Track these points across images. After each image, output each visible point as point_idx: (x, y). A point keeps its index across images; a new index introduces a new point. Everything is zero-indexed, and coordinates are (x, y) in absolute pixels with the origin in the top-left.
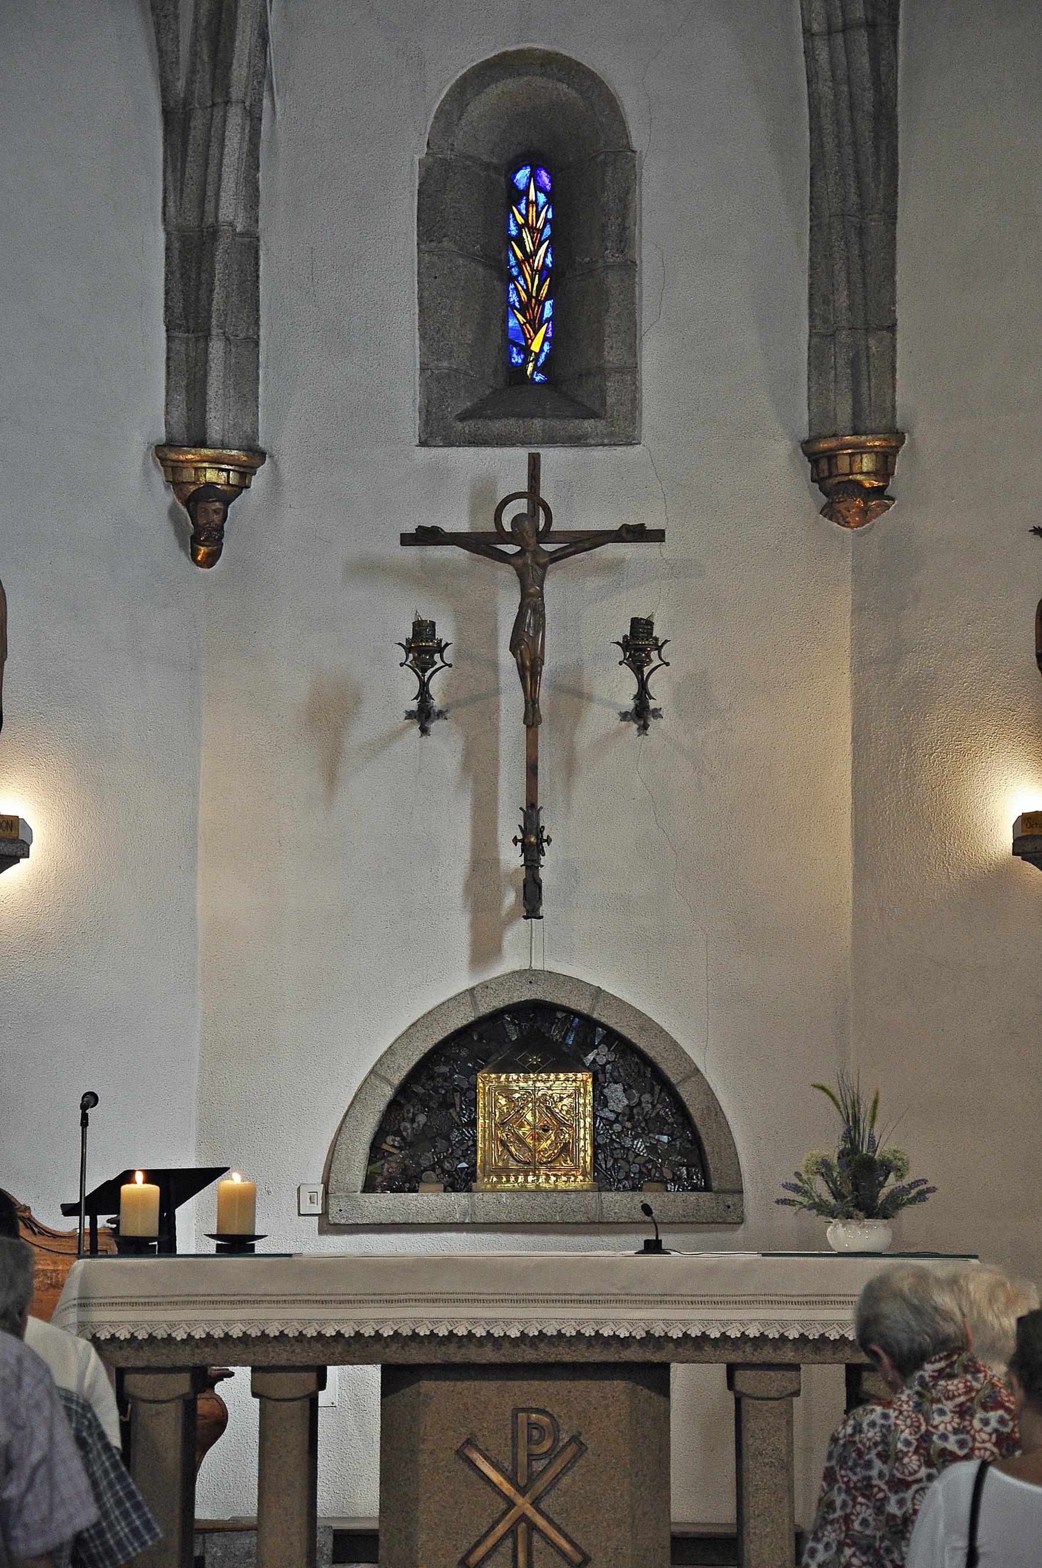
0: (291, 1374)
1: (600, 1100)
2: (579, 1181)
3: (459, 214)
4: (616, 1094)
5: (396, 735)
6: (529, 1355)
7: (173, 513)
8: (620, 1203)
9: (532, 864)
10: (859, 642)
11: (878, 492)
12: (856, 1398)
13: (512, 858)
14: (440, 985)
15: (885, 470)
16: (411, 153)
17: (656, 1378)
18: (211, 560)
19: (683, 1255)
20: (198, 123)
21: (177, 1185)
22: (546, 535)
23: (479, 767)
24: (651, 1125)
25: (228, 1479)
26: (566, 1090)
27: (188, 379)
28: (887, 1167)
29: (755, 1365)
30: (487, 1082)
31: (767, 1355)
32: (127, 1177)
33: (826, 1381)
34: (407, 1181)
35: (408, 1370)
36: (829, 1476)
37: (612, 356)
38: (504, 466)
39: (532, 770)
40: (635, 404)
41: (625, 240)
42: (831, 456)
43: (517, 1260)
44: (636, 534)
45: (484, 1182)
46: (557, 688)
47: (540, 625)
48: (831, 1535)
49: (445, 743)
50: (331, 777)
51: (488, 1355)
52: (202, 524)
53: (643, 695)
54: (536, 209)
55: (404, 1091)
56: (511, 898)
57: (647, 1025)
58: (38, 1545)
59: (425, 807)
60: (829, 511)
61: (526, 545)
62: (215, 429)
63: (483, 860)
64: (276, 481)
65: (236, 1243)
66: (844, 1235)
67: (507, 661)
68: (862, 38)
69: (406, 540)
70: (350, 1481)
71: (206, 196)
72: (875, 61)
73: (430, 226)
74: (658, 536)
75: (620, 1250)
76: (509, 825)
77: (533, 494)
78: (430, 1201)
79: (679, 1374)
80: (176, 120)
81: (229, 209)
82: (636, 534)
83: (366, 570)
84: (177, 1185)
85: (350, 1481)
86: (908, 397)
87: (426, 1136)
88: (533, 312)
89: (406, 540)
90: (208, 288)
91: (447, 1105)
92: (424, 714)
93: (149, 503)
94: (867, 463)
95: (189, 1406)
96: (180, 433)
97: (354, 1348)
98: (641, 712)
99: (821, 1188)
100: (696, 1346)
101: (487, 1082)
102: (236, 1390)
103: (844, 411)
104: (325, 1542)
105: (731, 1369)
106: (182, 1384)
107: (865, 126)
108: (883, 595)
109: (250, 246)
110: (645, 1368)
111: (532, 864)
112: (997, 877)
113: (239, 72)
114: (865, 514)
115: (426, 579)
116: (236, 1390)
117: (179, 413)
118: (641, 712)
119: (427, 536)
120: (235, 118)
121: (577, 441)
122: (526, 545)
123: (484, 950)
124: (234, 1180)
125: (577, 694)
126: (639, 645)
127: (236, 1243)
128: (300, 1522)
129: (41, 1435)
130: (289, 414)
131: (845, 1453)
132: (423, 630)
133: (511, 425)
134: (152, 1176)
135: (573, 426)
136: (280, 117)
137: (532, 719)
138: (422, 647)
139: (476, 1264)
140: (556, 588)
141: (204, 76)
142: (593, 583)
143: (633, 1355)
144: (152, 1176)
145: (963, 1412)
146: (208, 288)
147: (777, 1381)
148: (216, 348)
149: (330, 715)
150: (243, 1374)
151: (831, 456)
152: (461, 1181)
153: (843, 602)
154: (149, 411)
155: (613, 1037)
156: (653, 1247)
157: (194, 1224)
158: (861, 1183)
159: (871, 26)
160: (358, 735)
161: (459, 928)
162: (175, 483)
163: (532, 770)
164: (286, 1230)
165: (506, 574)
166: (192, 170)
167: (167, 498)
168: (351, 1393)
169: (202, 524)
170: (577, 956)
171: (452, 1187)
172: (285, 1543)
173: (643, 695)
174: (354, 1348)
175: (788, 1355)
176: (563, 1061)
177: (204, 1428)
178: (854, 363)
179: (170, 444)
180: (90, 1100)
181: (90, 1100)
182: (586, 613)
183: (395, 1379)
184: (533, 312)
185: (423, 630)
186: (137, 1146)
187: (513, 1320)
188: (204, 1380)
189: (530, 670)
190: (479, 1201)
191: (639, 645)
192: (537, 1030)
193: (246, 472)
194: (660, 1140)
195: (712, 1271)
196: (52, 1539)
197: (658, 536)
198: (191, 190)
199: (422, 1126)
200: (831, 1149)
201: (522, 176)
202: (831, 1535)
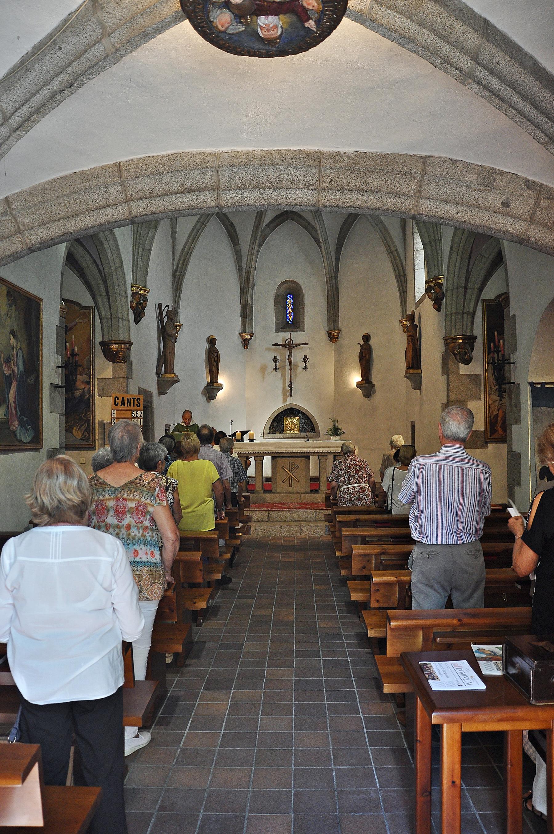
0: (260, 457)
1: (300, 421)
2: (297, 432)
3: (280, 301)
4: (302, 420)
5: (272, 372)
6: (291, 455)
7: (242, 342)
8: (303, 435)
9: (291, 389)
10: (335, 358)
11: (337, 338)
12: (335, 460)
13: (288, 388)
14: (278, 405)
15: (338, 335)
16: (274, 293)
17: (308, 458)
18: (247, 348)
19: (312, 442)
20: (245, 291)
21: (244, 433)
22: (292, 344)
23: (283, 376)
24: (307, 424)
25: (251, 471)
26: (296, 420)
27: (244, 324)
28: (339, 429)
29: (322, 456)
30: (285, 419)
31: (323, 454)
32: (237, 432)
33: (331, 458)
34: (275, 432)
35: (275, 457)
36: (333, 468)
37: (301, 320)
38: (286, 335)
39: (291, 376)
40: (304, 326)
41: (302, 305)
42: (331, 333)
43: (290, 442)
44: (305, 344)
45: (285, 432)
46: (294, 365)
47: (292, 356)
48: (332, 476)
49: (279, 373)
50: (263, 378)
51: (286, 455)
52: (246, 343)
53: (306, 366)
54: (290, 301)
55: (274, 420)
56: (288, 394)
57: (307, 411)
58: (225, 478)
59: (276, 382)
60: (331, 341)
61: (290, 346)
62: (247, 331)
63: (284, 389)
64: (255, 337)
65: (252, 441)
66: (333, 438)
67: (287, 361)
68: (334, 278)
69: (273, 345)
70: (268, 471)
71: (246, 300)
72: (335, 280)
73: (276, 303)
74: (308, 344)
75: (303, 441)
76: (288, 384)
77: (290, 339)
78: (278, 435)
79: (311, 457)
80: (242, 290)
81: (249, 301)
82: (305, 344)
83: (268, 349)
84: (244, 433)
85: (268, 471)
86: (341, 325)
87: (277, 426)
88: (290, 321)
89: (273, 345)
90: (247, 312)
91: (280, 422)
92: (276, 369)
93: (238, 341)
94: (336, 334)
95: (246, 462)
96: (242, 331)
97: (268, 454)
98: (306, 368)
99: (330, 432)
100: (313, 453)
101: (285, 419)
102: (252, 460)
103: (332, 328)
104: (264, 479)
105: (318, 456)
106: (245, 459)
107: (334, 290)
108: (339, 353)
109: (252, 306)
110: (306, 456)
111: (291, 389)
112: (354, 390)
113: (250, 284)
114: (336, 341)
115: (276, 350)
116: (252, 460)
117: (243, 328)
118: (306, 368)
119: (276, 345)
120: (250, 289)
121: (296, 331)
122: (290, 346)
123: (285, 401)
124: (251, 432)
125: (296, 366)
126: (305, 359)
127: (252, 441)
128: (261, 477)
129: (225, 464)
130: (258, 328)
131: (335, 466)
132: (276, 357)
133: (288, 329)
134: (240, 432)
135: (296, 329)
136: (257, 290)
137: (291, 369)
138: (276, 360)
139: (283, 443)
140: (294, 352)
141: (246, 284)
142: (299, 350)
143: (305, 455)
144: (240, 432)
145: (351, 461)
146: (247, 312)
147: (325, 458)
148: (247, 320)
149: (263, 369)
150: (253, 458)
151: (331, 333)
152: (282, 432)
153: (333, 352)
154: (238, 328)
155: (302, 412)
156: (308, 440)
157: (246, 438)
158: (336, 431)
159: (335, 277)
160: (267, 372)
161: (281, 398)
162: (242, 338)
163: (291, 376)
164: (258, 439)
165: (287, 349)
166: (244, 297)
167: (241, 340)
168: (267, 461)
169: (246, 343)
170: (297, 401)
171: (280, 433)
172: (259, 480)
173: (306, 366)
174: (268, 454)
175: (326, 454)
176: (295, 416)
177: (248, 465)
178: (334, 321)
179: (241, 333)
180: (232, 421)
181: (232, 421)
182: (298, 355)
183: (273, 458)
184: (290, 321)
185: (276, 357)
186: (238, 428)
187: (289, 450)
188: (248, 458)
189: (290, 363)
190: (284, 435)
191: (305, 359)
192: (292, 412)
193: (251, 337)
194: (309, 426)
195: (316, 443)
196: (227, 478)
197: (308, 344)
198: (244, 299)
199: (276, 425)
200: (331, 427)
201: (288, 296)
202: (332, 476)
